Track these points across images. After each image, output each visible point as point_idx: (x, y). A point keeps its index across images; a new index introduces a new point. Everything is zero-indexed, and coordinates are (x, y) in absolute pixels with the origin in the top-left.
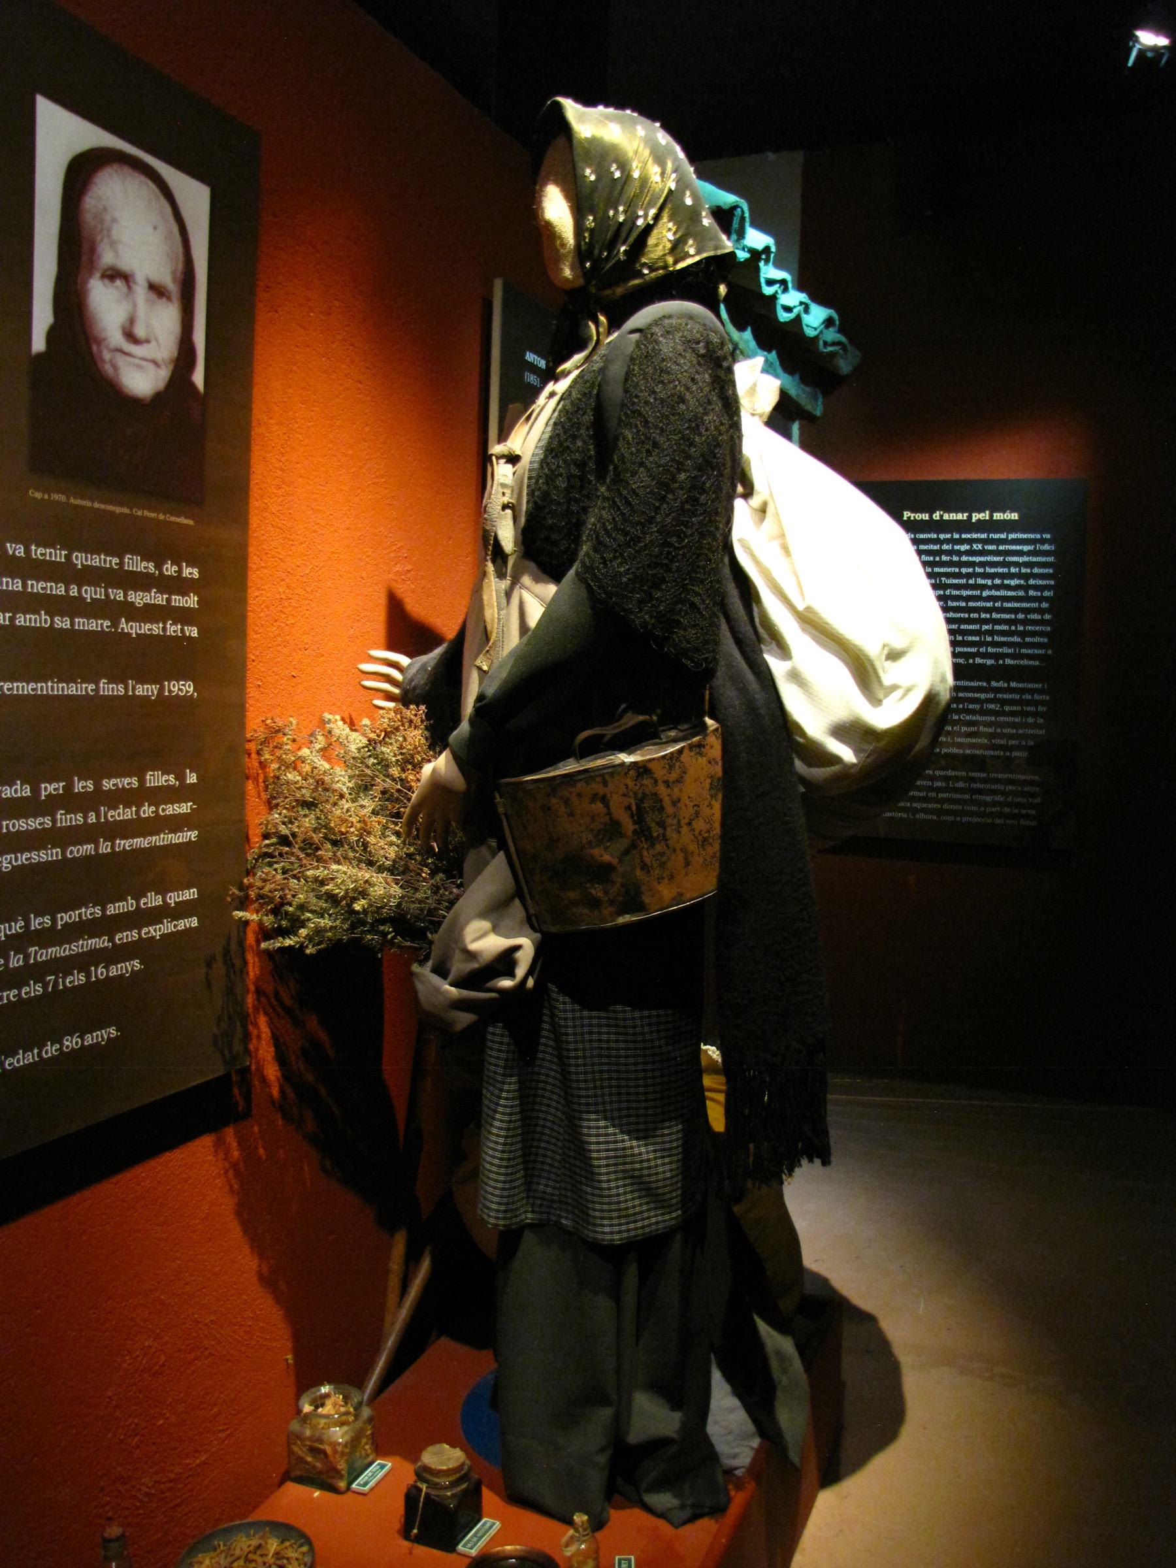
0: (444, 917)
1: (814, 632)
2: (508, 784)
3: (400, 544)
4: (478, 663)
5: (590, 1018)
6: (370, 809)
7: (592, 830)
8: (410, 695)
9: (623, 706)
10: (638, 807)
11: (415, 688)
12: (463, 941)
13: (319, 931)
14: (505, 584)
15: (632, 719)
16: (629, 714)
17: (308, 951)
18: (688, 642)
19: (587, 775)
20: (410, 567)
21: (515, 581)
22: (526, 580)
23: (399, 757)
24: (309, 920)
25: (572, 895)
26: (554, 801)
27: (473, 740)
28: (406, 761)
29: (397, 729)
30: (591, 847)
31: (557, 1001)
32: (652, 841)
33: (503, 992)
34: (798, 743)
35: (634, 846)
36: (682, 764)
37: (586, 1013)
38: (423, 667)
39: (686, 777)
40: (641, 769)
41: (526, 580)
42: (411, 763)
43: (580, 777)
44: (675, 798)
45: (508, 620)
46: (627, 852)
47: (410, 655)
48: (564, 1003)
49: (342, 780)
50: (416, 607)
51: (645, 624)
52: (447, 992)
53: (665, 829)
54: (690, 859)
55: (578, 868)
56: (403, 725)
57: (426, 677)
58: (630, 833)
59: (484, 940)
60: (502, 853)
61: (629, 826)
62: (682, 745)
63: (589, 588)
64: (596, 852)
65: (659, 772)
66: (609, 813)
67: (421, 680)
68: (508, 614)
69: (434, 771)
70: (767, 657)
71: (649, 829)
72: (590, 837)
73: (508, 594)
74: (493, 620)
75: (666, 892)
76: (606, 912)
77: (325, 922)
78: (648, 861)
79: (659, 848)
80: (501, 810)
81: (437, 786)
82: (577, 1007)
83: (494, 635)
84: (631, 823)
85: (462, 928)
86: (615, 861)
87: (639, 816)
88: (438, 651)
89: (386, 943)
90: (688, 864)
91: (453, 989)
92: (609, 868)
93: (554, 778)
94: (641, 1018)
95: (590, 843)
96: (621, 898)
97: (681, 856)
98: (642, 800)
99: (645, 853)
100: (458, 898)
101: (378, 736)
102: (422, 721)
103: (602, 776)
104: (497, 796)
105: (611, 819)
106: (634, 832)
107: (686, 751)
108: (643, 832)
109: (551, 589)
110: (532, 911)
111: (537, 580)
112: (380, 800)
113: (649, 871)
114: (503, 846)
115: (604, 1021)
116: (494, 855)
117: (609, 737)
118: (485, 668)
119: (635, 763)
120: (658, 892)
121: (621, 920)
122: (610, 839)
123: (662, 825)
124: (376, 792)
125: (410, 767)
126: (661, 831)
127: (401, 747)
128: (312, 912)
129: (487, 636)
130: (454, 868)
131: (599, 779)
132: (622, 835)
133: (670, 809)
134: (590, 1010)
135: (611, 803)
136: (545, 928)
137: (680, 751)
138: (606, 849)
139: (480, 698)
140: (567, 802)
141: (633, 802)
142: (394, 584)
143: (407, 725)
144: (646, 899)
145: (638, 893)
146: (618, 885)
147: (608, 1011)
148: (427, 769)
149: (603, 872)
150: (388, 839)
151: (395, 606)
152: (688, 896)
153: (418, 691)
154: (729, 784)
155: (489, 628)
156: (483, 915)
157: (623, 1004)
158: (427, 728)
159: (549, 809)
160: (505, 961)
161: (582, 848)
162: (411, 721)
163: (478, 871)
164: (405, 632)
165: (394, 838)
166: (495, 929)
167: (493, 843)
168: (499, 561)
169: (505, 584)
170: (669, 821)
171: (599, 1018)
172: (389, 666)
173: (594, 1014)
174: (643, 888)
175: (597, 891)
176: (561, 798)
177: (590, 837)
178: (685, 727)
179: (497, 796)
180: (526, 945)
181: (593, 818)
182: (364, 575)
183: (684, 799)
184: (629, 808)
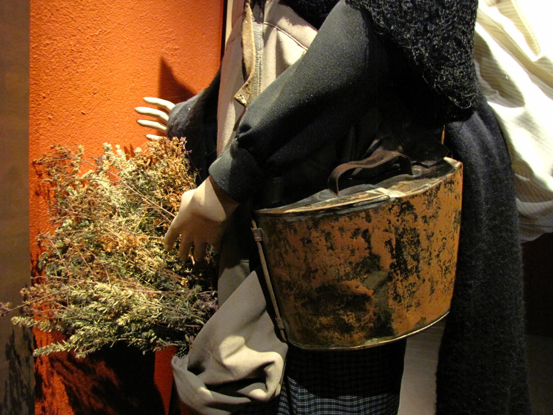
0: (202, 326)
1: (542, 83)
2: (266, 215)
3: (170, 30)
4: (237, 96)
5: (322, 403)
6: (139, 223)
7: (350, 263)
8: (173, 130)
9: (376, 142)
10: (398, 242)
11: (177, 125)
12: (219, 355)
13: (88, 338)
14: (262, 28)
15: (384, 155)
16: (380, 150)
17: (78, 356)
18: (455, 79)
19: (352, 210)
20: (177, 47)
21: (272, 24)
22: (284, 23)
23: (163, 181)
24: (79, 327)
25: (324, 320)
26: (315, 234)
27: (235, 171)
28: (169, 184)
29: (162, 157)
30: (348, 279)
31: (296, 392)
32: (406, 272)
33: (255, 401)
34: (519, 180)
35: (390, 278)
36: (420, 197)
37: (318, 400)
38: (185, 108)
39: (440, 212)
40: (405, 206)
41: (284, 23)
42: (173, 187)
43: (344, 212)
44: (430, 232)
45: (265, 59)
46: (382, 284)
47: (175, 102)
48: (302, 394)
49: (118, 198)
50: (181, 74)
51: (421, 57)
52: (203, 394)
53: (418, 262)
54: (435, 287)
55: (333, 297)
56: (166, 153)
57: (186, 115)
58: (387, 267)
59: (240, 356)
60: (254, 273)
61: (387, 260)
62: (437, 181)
63: (366, 15)
64: (353, 283)
65: (420, 208)
66: (370, 248)
67: (183, 119)
68: (265, 53)
69: (193, 200)
70: (490, 103)
71: (405, 262)
72: (348, 269)
73: (266, 37)
74: (251, 58)
75: (412, 317)
76: (356, 336)
77: (92, 329)
78: (400, 291)
79: (412, 279)
80: (258, 238)
81: (197, 216)
82: (312, 396)
83: (253, 71)
84: (389, 255)
85: (218, 343)
86: (370, 292)
87: (397, 251)
88: (194, 99)
89: (149, 345)
90: (433, 291)
91: (208, 392)
92: (365, 298)
93: (317, 212)
94: (364, 403)
95: (347, 275)
96: (371, 325)
97: (428, 284)
98: (401, 236)
99: (399, 284)
100: (212, 312)
101: (145, 162)
102: (183, 151)
103: (367, 211)
104: (254, 224)
105: (370, 253)
106: (392, 266)
107: (442, 187)
108: (400, 265)
109: (309, 34)
110: (281, 326)
111: (294, 23)
112: (146, 215)
113: (400, 301)
114: (255, 266)
115: (334, 406)
116: (247, 274)
117: (359, 170)
118: (244, 101)
119: (399, 199)
120: (406, 318)
121: (369, 343)
122: (368, 272)
123: (416, 258)
124: (143, 209)
125: (171, 189)
126: (415, 263)
127: (164, 172)
128: (81, 320)
129: (245, 74)
130: (207, 276)
131: (363, 214)
132: (379, 268)
133: (424, 243)
134: (322, 397)
135: (372, 240)
136: (294, 344)
137: (438, 188)
138: (363, 281)
139: (241, 128)
140: (328, 236)
141: (393, 236)
142: (165, 56)
143: (170, 153)
144: (395, 325)
145: (388, 316)
146: (371, 313)
147: (338, 399)
148: (187, 196)
149: (358, 302)
150: (153, 250)
151: (166, 73)
152: (428, 320)
153: (180, 127)
154: (468, 215)
155: (247, 65)
156: (236, 332)
157: (351, 394)
158: (186, 157)
159: (309, 241)
160: (260, 375)
161: (340, 279)
162: (173, 150)
163: (233, 288)
164: (172, 88)
165: (157, 249)
166: (248, 343)
167: (246, 263)
168: (257, 6)
169: (262, 28)
170: (422, 254)
171: (330, 403)
172: (157, 109)
173: (326, 400)
174: (394, 316)
175: (350, 318)
176: (323, 232)
177: (348, 269)
178: (430, 163)
179: (254, 224)
180: (276, 358)
181: (353, 251)
182: (144, 46)
183: (437, 232)
184: (389, 242)
